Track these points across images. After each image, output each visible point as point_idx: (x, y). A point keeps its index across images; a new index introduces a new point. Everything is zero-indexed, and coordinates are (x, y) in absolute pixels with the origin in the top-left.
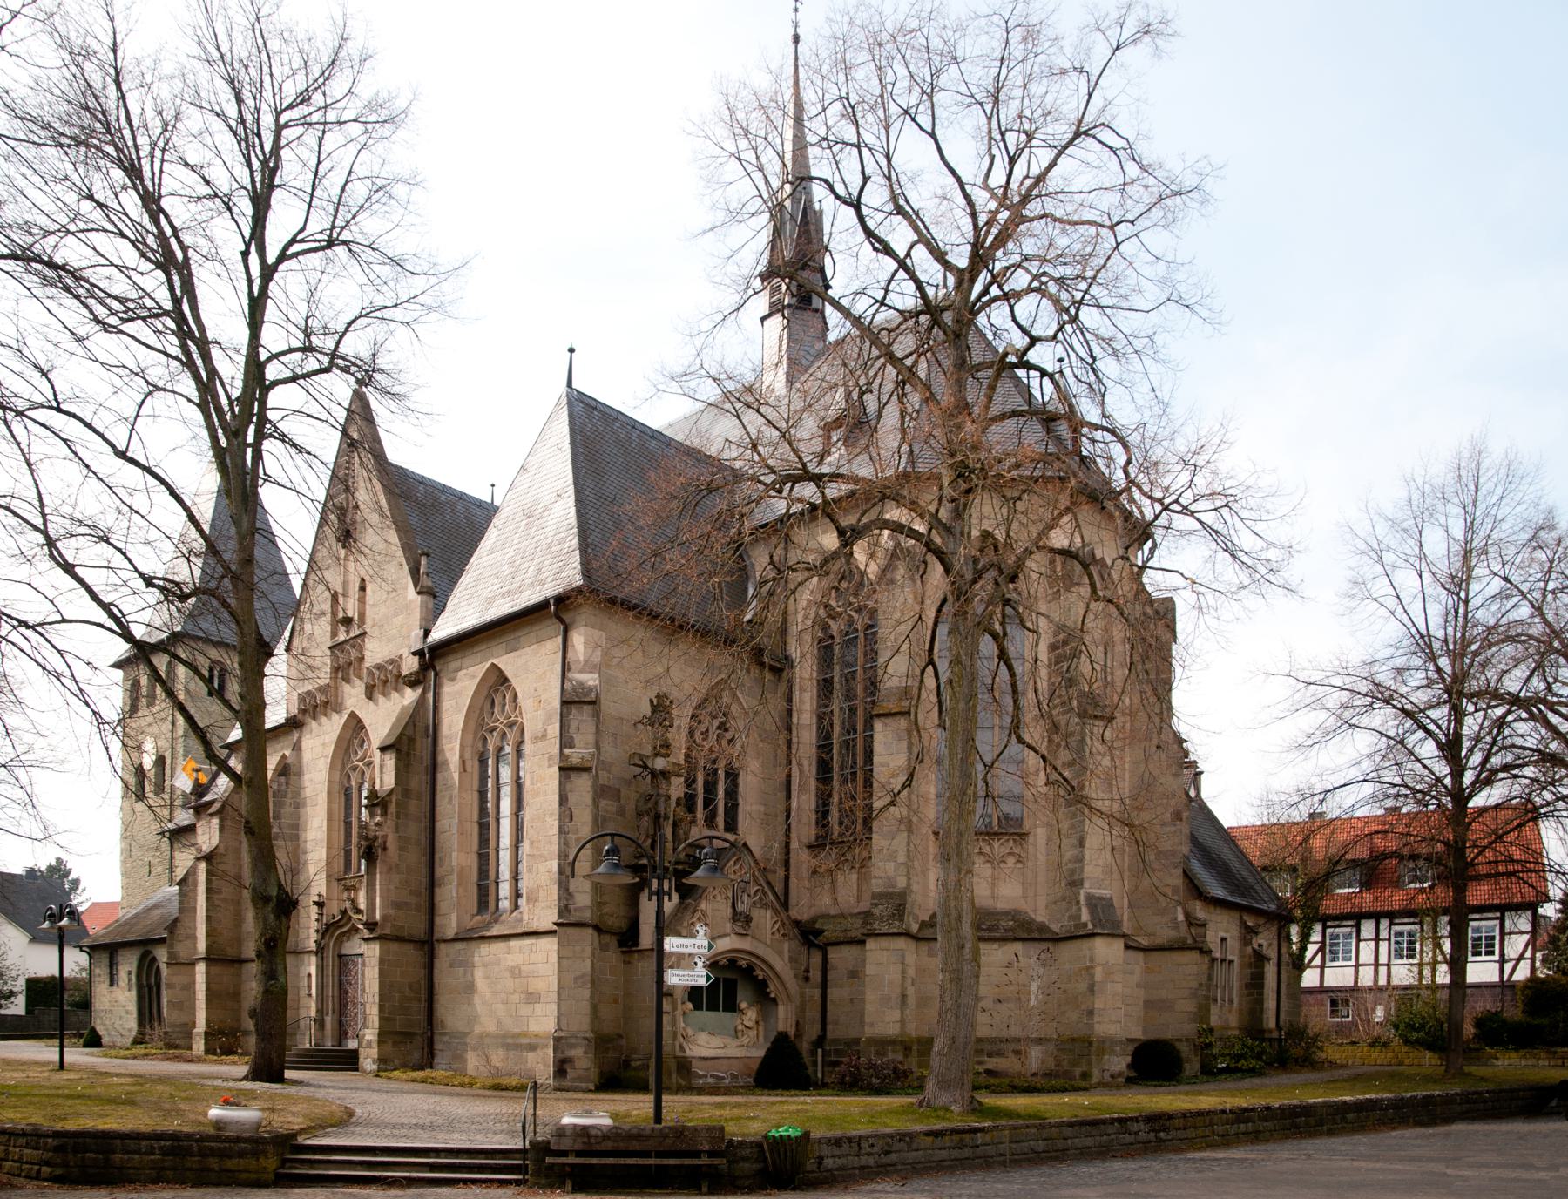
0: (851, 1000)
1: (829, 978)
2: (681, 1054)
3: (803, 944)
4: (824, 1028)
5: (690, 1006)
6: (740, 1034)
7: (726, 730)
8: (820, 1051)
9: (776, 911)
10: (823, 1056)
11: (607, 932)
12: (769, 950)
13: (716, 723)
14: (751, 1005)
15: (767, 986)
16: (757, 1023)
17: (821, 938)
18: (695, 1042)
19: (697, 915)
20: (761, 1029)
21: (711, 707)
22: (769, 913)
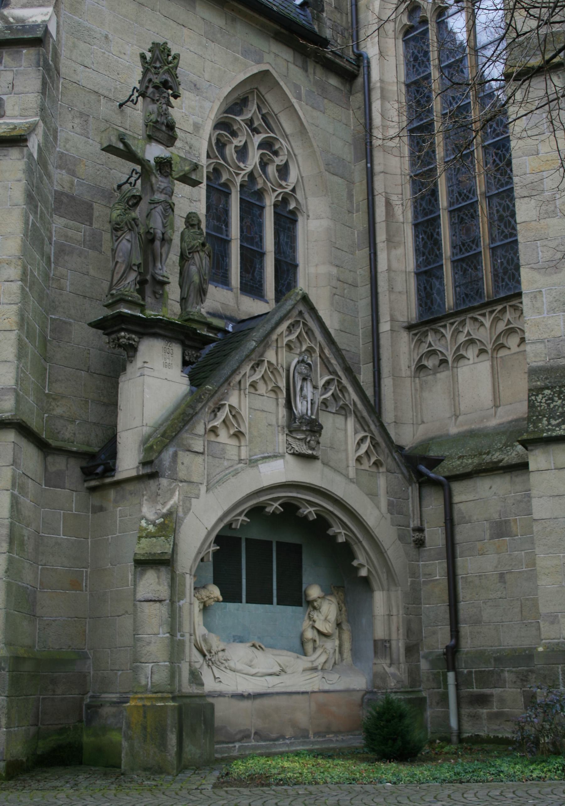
0: (502, 576)
1: (459, 538)
2: (194, 690)
3: (410, 482)
4: (455, 632)
5: (215, 592)
6: (309, 647)
7: (276, 153)
8: (451, 676)
9: (362, 422)
10: (457, 687)
11: (60, 451)
12: (353, 487)
13: (258, 139)
14: (327, 592)
15: (353, 557)
16: (339, 625)
17: (439, 468)
18: (223, 665)
19: (222, 415)
20: (346, 636)
21: (251, 111)
22: (351, 423)
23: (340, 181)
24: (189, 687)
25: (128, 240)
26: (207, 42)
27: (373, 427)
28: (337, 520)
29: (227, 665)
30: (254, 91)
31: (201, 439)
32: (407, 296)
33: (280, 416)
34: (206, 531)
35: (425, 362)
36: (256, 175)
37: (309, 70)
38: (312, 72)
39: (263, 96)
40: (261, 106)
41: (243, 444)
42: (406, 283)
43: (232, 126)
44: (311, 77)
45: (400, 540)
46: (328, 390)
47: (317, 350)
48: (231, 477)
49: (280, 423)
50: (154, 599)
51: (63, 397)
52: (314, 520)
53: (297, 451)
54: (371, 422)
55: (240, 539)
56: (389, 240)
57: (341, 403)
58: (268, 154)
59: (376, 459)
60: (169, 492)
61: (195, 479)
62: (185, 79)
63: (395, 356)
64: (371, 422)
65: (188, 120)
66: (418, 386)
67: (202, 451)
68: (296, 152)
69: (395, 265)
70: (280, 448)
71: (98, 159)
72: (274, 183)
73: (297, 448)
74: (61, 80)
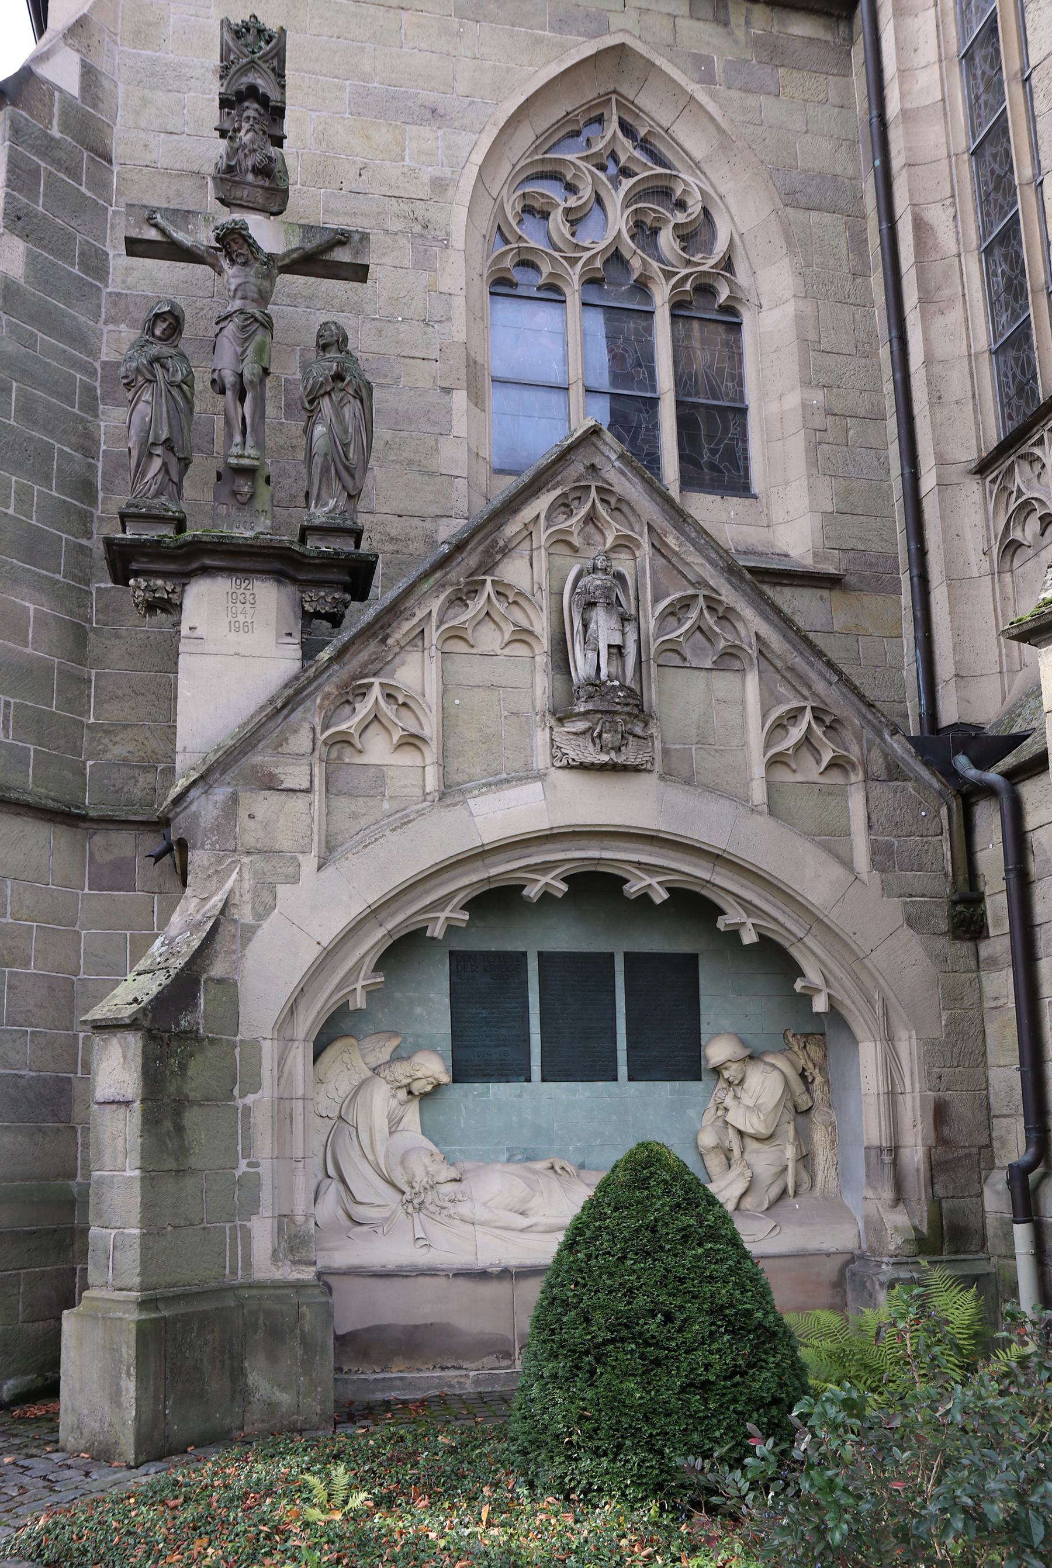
23: (828, 218)
24: (274, 1269)
25: (146, 402)
26: (461, 26)
27: (820, 686)
28: (730, 899)
29: (452, 1212)
30: (610, 99)
31: (305, 761)
32: (975, 404)
33: (539, 691)
34: (319, 948)
35: (1016, 534)
36: (627, 255)
37: (733, 19)
38: (742, 20)
39: (632, 103)
40: (629, 119)
41: (428, 760)
42: (972, 377)
43: (565, 177)
44: (740, 34)
45: (910, 925)
46: (683, 621)
47: (645, 542)
48: (387, 833)
49: (538, 708)
50: (117, 1099)
51: (125, 727)
52: (665, 902)
53: (574, 760)
54: (813, 676)
55: (524, 954)
56: (924, 301)
57: (722, 644)
58: (650, 209)
59: (832, 754)
60: (215, 878)
61: (285, 843)
62: (409, 103)
63: (952, 536)
64: (813, 676)
65: (416, 178)
66: (1009, 590)
67: (305, 785)
68: (722, 190)
69: (943, 348)
70: (540, 758)
71: (200, 288)
72: (674, 263)
73: (572, 754)
74: (116, 168)
